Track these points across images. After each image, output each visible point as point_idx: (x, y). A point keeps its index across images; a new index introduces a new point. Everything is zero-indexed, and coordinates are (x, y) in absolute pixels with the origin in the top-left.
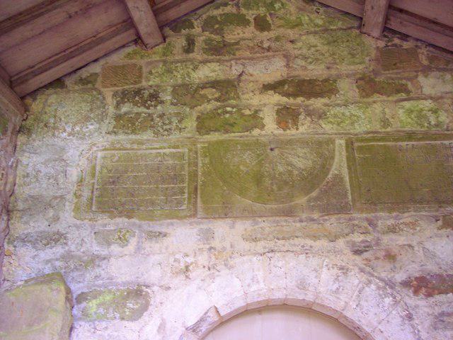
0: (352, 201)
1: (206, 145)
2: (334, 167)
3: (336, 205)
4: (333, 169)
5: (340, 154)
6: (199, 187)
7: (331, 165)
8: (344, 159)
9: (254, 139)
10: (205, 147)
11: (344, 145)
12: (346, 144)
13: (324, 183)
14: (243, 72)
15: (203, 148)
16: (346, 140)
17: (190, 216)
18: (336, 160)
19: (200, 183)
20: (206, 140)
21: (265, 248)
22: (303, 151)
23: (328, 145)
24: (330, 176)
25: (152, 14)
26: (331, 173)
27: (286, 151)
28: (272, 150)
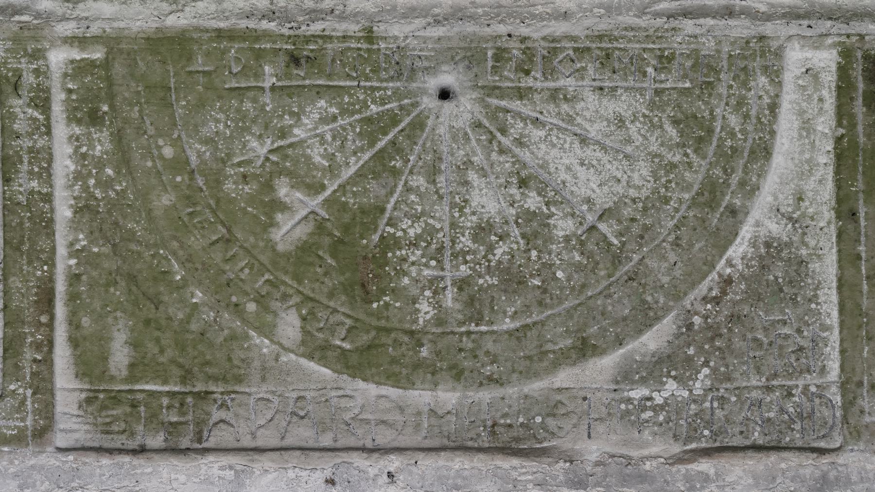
0: (843, 386)
1: (97, 54)
2: (765, 198)
3: (759, 404)
4: (755, 214)
5: (807, 127)
6: (61, 287)
7: (750, 190)
8: (825, 157)
9: (353, 28)
10: (92, 64)
11: (830, 78)
12: (843, 71)
13: (708, 284)
14: (266, 122)
15: (79, 69)
16: (846, 53)
17: (19, 440)
18: (779, 160)
19: (64, 262)
20: (95, 29)
21: (839, 434)
22: (611, 107)
23: (744, 76)
24: (738, 250)
25: (53, 131)
26: (746, 231)
27: (516, 105)
28: (445, 94)
